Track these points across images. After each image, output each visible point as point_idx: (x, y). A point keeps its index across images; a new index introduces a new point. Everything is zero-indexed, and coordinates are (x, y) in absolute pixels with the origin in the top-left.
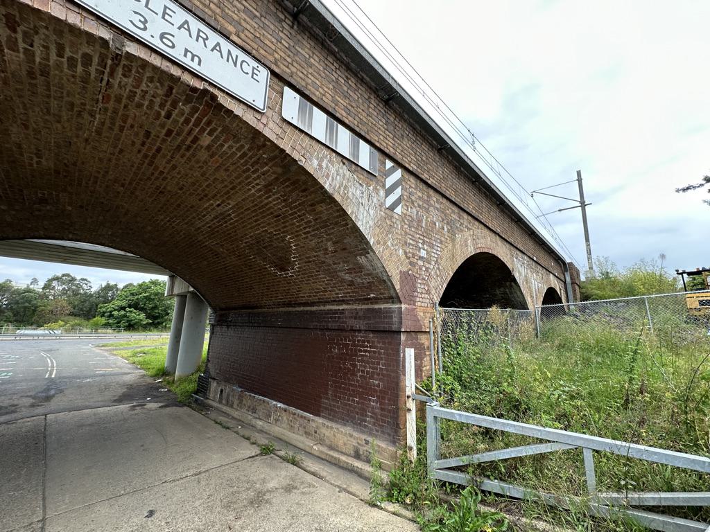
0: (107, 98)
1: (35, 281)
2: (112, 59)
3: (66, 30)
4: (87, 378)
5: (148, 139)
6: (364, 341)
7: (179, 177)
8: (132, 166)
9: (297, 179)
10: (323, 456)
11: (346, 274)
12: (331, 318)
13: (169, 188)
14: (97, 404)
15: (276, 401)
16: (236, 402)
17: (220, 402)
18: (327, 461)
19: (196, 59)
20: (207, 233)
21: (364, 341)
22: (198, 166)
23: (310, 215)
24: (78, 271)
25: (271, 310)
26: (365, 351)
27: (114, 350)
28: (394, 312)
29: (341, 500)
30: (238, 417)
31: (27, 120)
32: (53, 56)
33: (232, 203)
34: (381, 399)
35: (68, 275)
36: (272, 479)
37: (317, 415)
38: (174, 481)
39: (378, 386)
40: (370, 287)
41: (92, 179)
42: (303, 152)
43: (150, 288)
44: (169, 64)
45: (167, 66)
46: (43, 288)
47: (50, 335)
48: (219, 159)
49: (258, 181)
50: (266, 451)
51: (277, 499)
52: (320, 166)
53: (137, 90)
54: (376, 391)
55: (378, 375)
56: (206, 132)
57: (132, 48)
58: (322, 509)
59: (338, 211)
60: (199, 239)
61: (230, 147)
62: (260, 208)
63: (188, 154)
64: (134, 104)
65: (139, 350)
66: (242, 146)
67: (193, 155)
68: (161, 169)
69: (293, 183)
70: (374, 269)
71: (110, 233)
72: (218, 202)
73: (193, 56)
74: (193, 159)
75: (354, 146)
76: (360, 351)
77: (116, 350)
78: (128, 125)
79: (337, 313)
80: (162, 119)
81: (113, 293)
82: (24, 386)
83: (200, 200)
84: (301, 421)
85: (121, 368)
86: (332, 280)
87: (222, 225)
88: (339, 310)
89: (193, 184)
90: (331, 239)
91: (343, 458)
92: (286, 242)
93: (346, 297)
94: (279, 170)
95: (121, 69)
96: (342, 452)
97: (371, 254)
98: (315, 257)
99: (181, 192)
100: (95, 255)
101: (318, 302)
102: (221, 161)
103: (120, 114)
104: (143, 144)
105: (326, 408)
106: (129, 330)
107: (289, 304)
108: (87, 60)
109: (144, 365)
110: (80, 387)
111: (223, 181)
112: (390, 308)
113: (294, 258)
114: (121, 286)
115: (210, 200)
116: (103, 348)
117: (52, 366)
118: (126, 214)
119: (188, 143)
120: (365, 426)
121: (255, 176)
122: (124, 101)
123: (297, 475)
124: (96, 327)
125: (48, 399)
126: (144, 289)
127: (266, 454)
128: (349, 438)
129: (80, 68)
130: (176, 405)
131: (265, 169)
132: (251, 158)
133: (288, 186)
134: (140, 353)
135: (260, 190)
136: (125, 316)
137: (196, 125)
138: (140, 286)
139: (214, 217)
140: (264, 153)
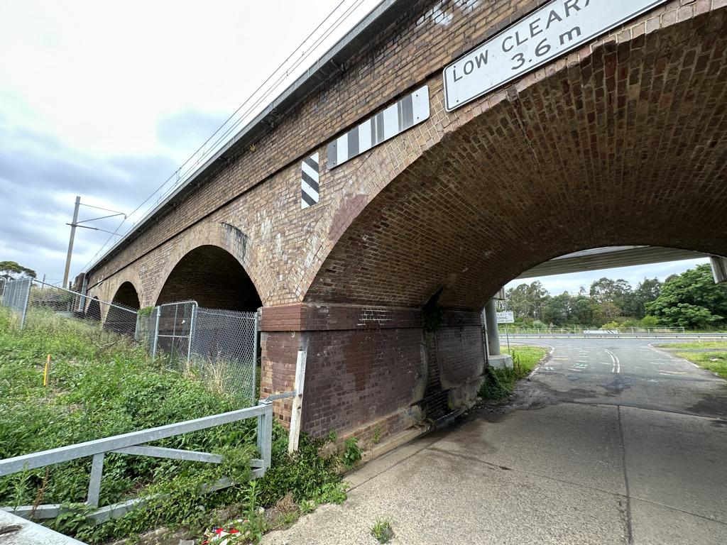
0: (530, 135)
1: (582, 289)
2: (516, 107)
4: (651, 378)
5: (578, 137)
7: (632, 148)
8: (582, 168)
14: (668, 408)
19: (574, 33)
22: (645, 122)
27: (677, 351)
31: (504, 184)
32: (490, 137)
35: (604, 279)
41: (561, 197)
43: (701, 276)
44: (551, 67)
45: (551, 70)
46: (590, 294)
47: (609, 335)
53: (543, 110)
56: (628, 84)
57: (521, 87)
60: (715, 199)
63: (625, 120)
64: (549, 122)
65: (711, 353)
68: (608, 153)
71: (604, 233)
72: (709, 142)
73: (569, 34)
77: (680, 351)
78: (556, 140)
80: (577, 112)
81: (656, 288)
82: (597, 376)
83: (679, 154)
85: (691, 373)
89: (655, 144)
95: (524, 108)
99: (647, 160)
100: (607, 257)
102: (671, 95)
103: (545, 137)
104: (577, 144)
106: (693, 329)
108: (504, 121)
114: (662, 280)
115: (692, 147)
116: (664, 349)
117: (616, 363)
118: (607, 211)
119: (616, 110)
124: (650, 326)
125: (618, 391)
126: (692, 279)
129: (504, 131)
134: (714, 357)
136: (679, 313)
138: (685, 275)
139: (718, 163)
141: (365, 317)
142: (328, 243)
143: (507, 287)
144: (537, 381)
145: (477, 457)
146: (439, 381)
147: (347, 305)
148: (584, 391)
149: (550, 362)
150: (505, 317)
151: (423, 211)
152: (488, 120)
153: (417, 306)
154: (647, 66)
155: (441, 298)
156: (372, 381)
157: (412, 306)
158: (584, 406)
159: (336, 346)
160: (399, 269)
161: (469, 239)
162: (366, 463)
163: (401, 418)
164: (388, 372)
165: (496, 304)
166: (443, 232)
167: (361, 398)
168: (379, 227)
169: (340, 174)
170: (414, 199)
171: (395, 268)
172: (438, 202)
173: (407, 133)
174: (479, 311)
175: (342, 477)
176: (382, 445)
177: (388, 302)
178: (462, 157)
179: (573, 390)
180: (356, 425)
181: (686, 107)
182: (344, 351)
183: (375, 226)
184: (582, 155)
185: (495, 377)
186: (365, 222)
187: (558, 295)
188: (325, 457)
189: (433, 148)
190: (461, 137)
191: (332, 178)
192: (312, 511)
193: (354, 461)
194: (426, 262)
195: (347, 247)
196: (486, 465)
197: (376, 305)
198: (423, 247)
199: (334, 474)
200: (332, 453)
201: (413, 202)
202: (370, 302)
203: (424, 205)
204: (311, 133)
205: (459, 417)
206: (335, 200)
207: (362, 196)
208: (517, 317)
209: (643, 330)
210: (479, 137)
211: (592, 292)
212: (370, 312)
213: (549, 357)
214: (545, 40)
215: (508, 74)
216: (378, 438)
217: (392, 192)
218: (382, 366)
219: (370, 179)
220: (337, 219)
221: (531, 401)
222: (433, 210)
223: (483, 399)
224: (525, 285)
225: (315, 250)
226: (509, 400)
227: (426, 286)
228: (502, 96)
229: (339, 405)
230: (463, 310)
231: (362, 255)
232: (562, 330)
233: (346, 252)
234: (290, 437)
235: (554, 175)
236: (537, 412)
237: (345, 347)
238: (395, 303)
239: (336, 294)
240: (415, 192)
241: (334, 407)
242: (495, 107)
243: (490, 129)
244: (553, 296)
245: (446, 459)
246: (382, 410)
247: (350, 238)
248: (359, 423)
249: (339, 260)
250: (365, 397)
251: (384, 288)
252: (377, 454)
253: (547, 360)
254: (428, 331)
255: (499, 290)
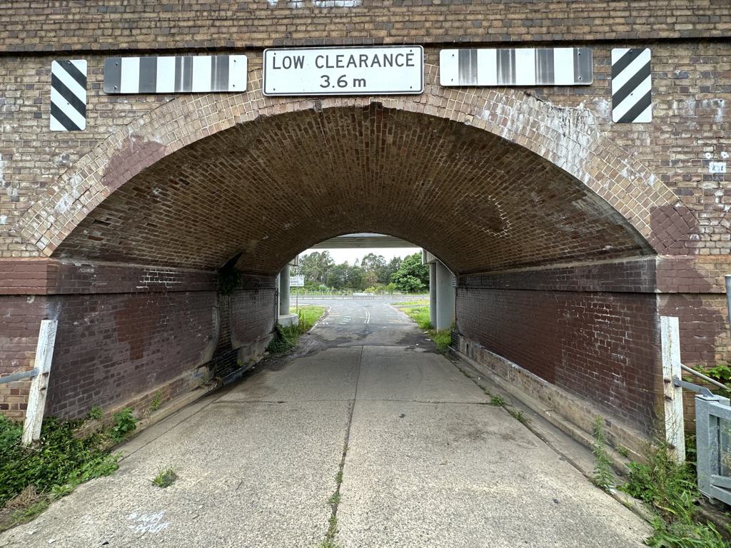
0: (328, 140)
1: (357, 260)
3: (296, 115)
6: (602, 306)
9: (472, 139)
10: (556, 424)
11: (565, 224)
12: (559, 278)
13: (386, 182)
15: (512, 361)
16: (479, 358)
17: (468, 355)
18: (561, 430)
20: (426, 208)
21: (602, 306)
23: (500, 169)
24: (377, 251)
25: (499, 272)
26: (604, 318)
28: (643, 266)
29: (559, 466)
30: (481, 371)
32: (299, 133)
33: (432, 180)
34: (629, 375)
36: (494, 425)
37: (552, 381)
38: (420, 402)
39: (624, 361)
40: (601, 237)
42: (469, 110)
44: (346, 100)
48: (77, 284)
49: (441, 154)
50: (496, 402)
51: (492, 441)
52: (493, 115)
54: (621, 367)
55: (623, 348)
57: (326, 104)
58: (534, 464)
59: (527, 156)
61: (408, 136)
62: (454, 177)
63: (385, 154)
66: (415, 131)
67: (388, 153)
69: (470, 145)
70: (601, 213)
74: (390, 156)
75: (544, 64)
76: (598, 317)
79: (565, 272)
82: (355, 327)
83: (409, 184)
84: (535, 385)
85: (403, 320)
86: (551, 235)
87: (432, 200)
88: (567, 268)
89: (399, 174)
90: (533, 189)
91: (578, 432)
92: (489, 202)
93: (574, 252)
94: (453, 138)
96: (579, 427)
97: (590, 195)
98: (523, 211)
101: (544, 261)
104: (358, 159)
105: (562, 378)
107: (515, 265)
109: (418, 319)
110: (379, 331)
111: (416, 165)
112: (637, 262)
113: (503, 216)
114: (402, 259)
115: (415, 182)
118: (373, 209)
120: (609, 406)
121: (436, 150)
122: (336, 138)
123: (520, 430)
124: (391, 290)
125: (365, 336)
126: (416, 259)
127: (496, 405)
128: (587, 414)
130: (434, 352)
131: (441, 142)
132: (426, 138)
133: (467, 149)
134: (416, 310)
135: (446, 162)
136: (407, 282)
137: (379, 131)
138: (414, 256)
140: (434, 129)
141: (147, 279)
142: (101, 188)
143: (301, 255)
144: (315, 334)
145: (260, 399)
146: (230, 341)
147: (122, 265)
148: (345, 338)
149: (327, 319)
150: (297, 280)
151: (230, 177)
152: (298, 118)
153: (213, 269)
154: (396, 127)
155: (239, 262)
156: (153, 348)
157: (207, 268)
158: (343, 349)
159: (105, 312)
160: (196, 230)
161: (273, 211)
162: (141, 431)
163: (186, 381)
164: (173, 337)
165: (290, 268)
166: (248, 200)
167: (137, 367)
168: (177, 183)
169: (124, 105)
170: (221, 163)
171: (191, 228)
172: (246, 172)
173: (221, 96)
174: (275, 275)
175: (110, 452)
176: (162, 411)
177: (178, 263)
178: (273, 140)
179: (339, 338)
180: (130, 396)
181: (413, 159)
182: (115, 318)
183: (171, 181)
184: (360, 167)
185: (283, 333)
186: (159, 175)
187: (340, 264)
188: (85, 437)
189: (247, 124)
190: (274, 123)
191: (111, 106)
192: (69, 493)
193: (126, 431)
194: (227, 226)
195: (132, 198)
196: (266, 403)
197: (163, 266)
198: (226, 211)
199: (98, 451)
200: (94, 431)
201: (221, 166)
202: (155, 262)
203: (231, 172)
204: (73, 26)
205: (247, 371)
206: (115, 137)
207: (159, 145)
208: (307, 281)
209: (387, 293)
210: (290, 129)
211: (363, 264)
212: (155, 274)
213: (327, 314)
214: (345, 76)
215: (315, 87)
216: (156, 404)
217: (197, 151)
218: (167, 331)
219: (170, 128)
220: (116, 163)
221: (308, 349)
222: (240, 179)
223: (270, 353)
224: (317, 253)
225: (76, 194)
226: (292, 351)
227: (225, 250)
228: (310, 105)
229: (106, 378)
230: (260, 274)
231: (150, 210)
232: (339, 292)
233: (128, 203)
234: (25, 427)
235: (343, 175)
236: (310, 358)
237: (117, 313)
238: (187, 264)
239: (107, 250)
240: (224, 158)
241: (99, 381)
242: (304, 111)
243: (299, 126)
244: (337, 264)
245: (232, 407)
246: (161, 378)
247: (136, 189)
248: (133, 394)
249: (117, 211)
250: (143, 365)
251: (174, 248)
252: (156, 420)
253: (324, 317)
254: (223, 294)
255: (294, 258)
